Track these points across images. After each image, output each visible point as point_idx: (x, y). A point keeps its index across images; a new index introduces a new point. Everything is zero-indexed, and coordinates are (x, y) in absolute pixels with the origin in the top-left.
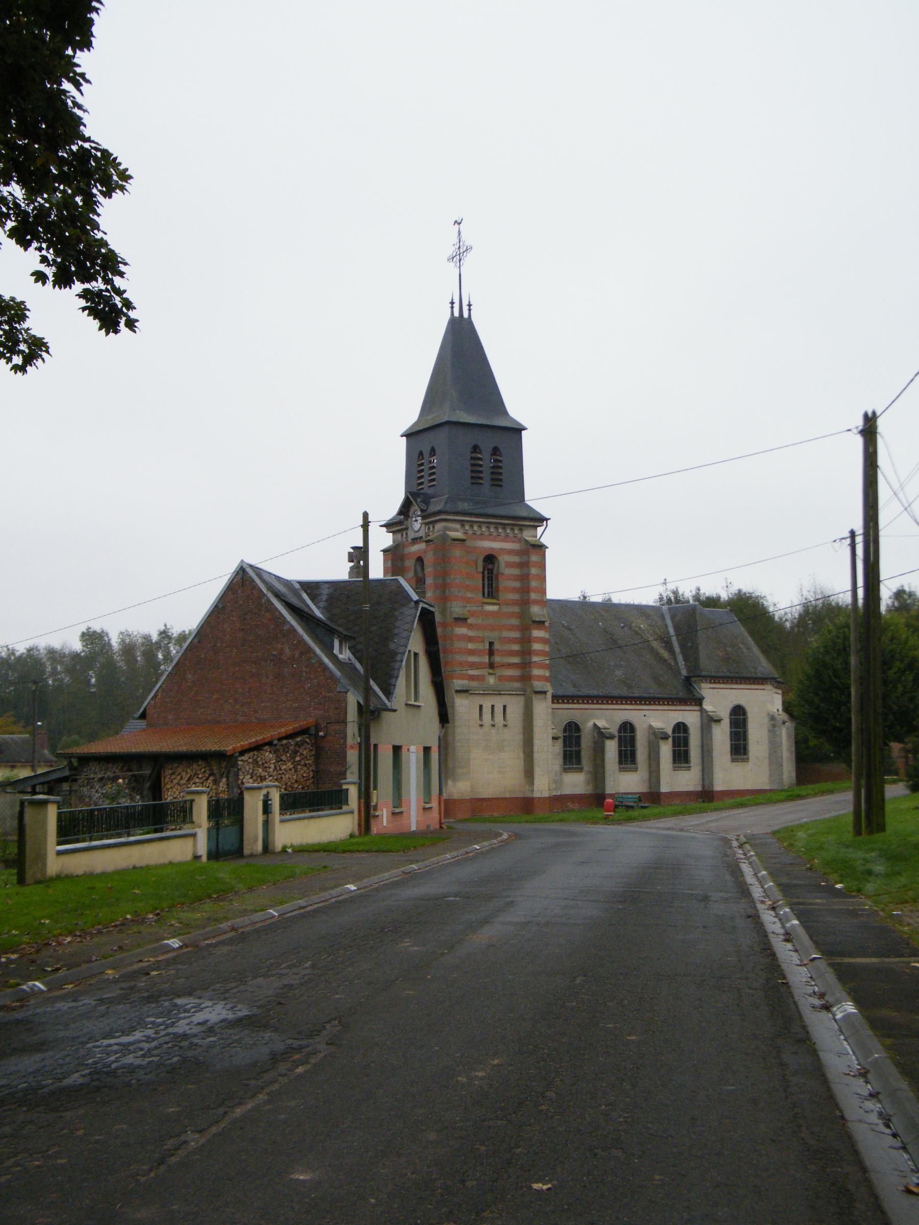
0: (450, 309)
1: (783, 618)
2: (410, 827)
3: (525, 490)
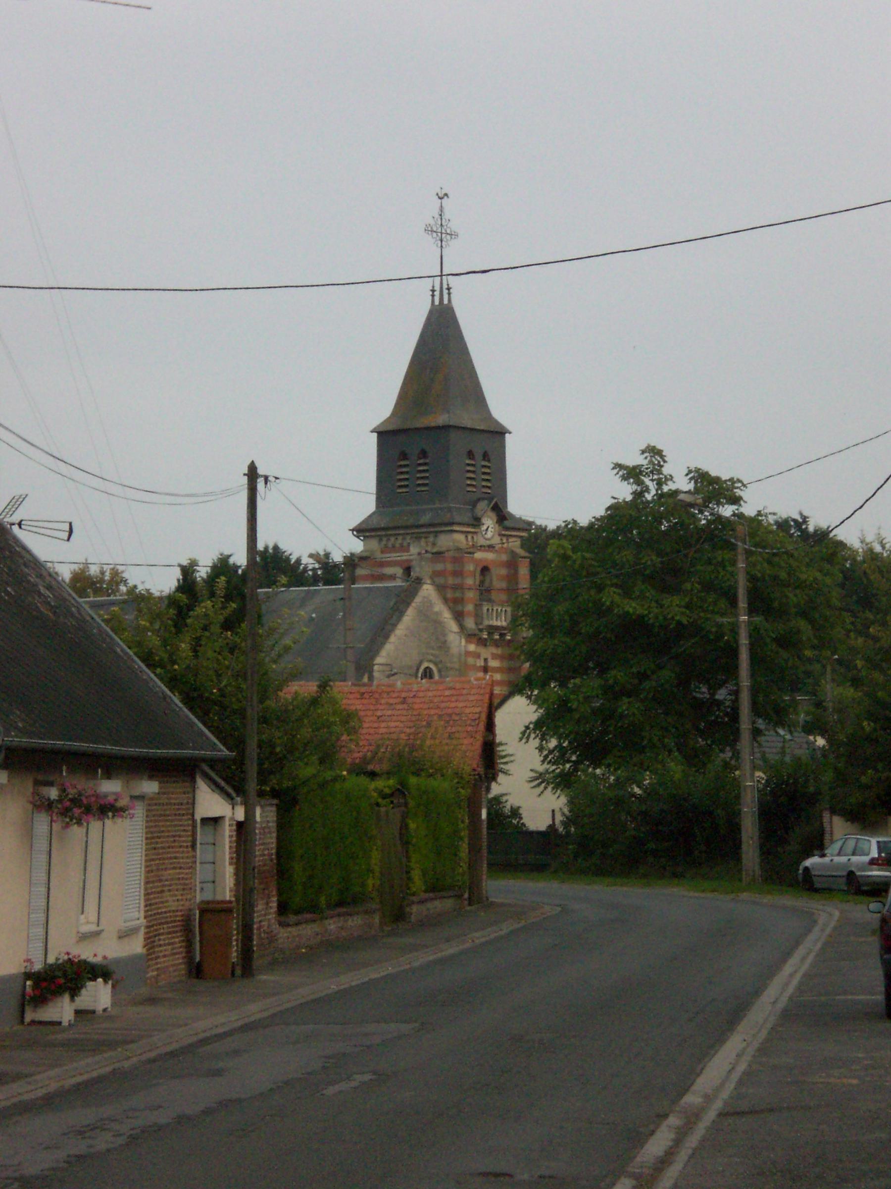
0: (430, 298)
1: (597, 675)
2: (225, 896)
3: (508, 490)
